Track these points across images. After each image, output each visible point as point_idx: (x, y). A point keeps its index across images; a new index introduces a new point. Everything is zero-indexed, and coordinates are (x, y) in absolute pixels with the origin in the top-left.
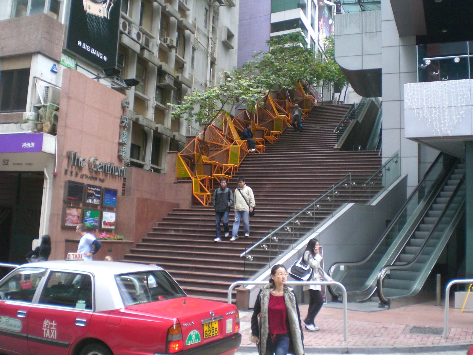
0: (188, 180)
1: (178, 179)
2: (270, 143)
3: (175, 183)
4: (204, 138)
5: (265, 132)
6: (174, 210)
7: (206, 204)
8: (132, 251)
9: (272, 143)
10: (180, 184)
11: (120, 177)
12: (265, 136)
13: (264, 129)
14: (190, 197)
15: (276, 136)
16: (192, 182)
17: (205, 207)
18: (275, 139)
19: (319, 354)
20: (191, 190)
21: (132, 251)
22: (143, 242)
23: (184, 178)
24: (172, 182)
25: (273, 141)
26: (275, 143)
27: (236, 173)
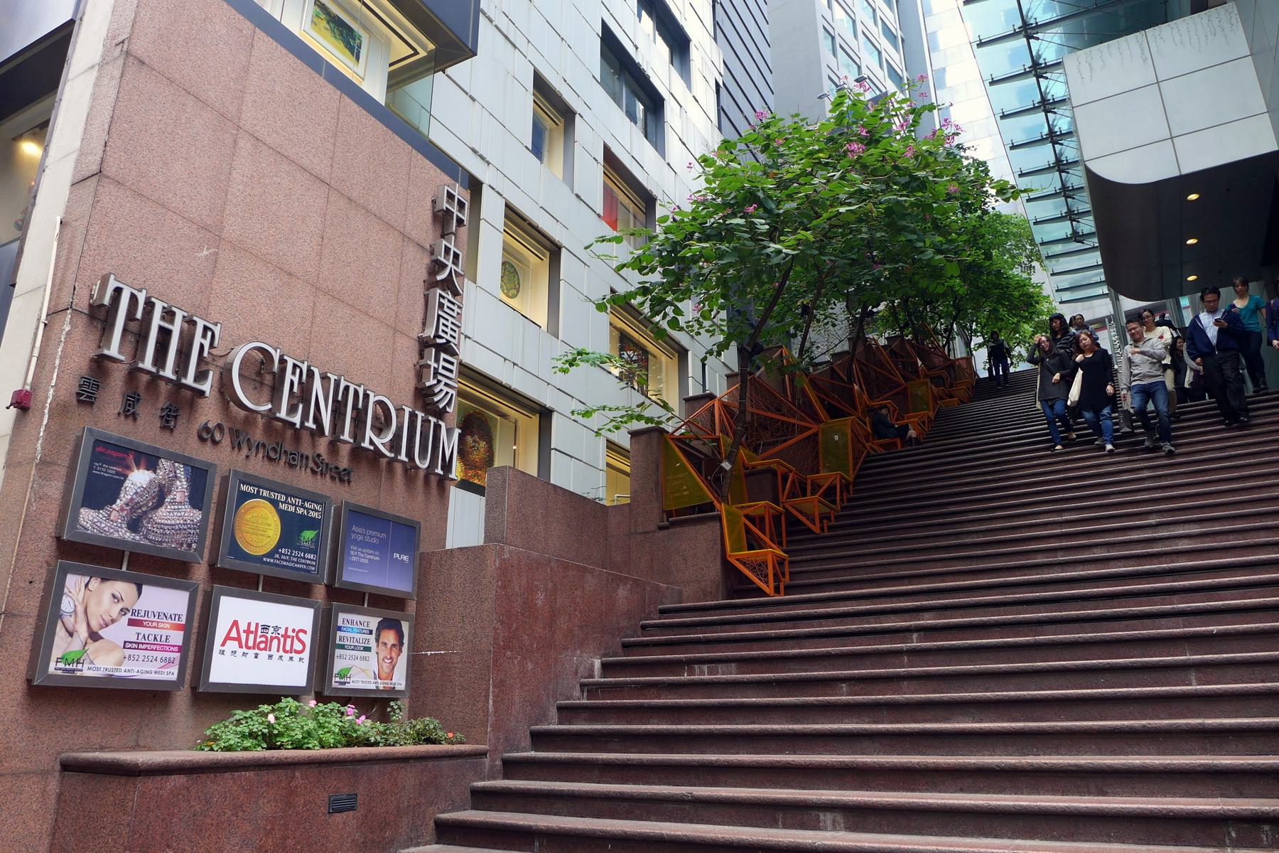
0: (702, 512)
1: (670, 514)
2: (809, 531)
3: (661, 528)
4: (342, 647)
5: (785, 479)
6: (644, 627)
7: (822, 529)
8: (483, 798)
9: (816, 529)
10: (678, 529)
11: (1045, 155)
12: (783, 498)
13: (774, 466)
14: (714, 570)
15: (830, 493)
16: (719, 518)
17: (818, 539)
18: (828, 510)
19: (1144, 848)
20: (718, 546)
21: (483, 798)
22: (560, 723)
23: (692, 510)
24: (653, 527)
25: (821, 519)
26: (830, 528)
27: (849, 500)
